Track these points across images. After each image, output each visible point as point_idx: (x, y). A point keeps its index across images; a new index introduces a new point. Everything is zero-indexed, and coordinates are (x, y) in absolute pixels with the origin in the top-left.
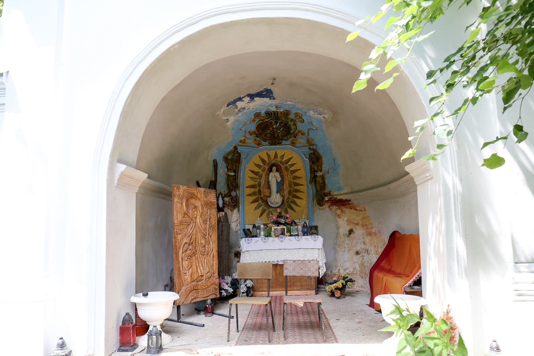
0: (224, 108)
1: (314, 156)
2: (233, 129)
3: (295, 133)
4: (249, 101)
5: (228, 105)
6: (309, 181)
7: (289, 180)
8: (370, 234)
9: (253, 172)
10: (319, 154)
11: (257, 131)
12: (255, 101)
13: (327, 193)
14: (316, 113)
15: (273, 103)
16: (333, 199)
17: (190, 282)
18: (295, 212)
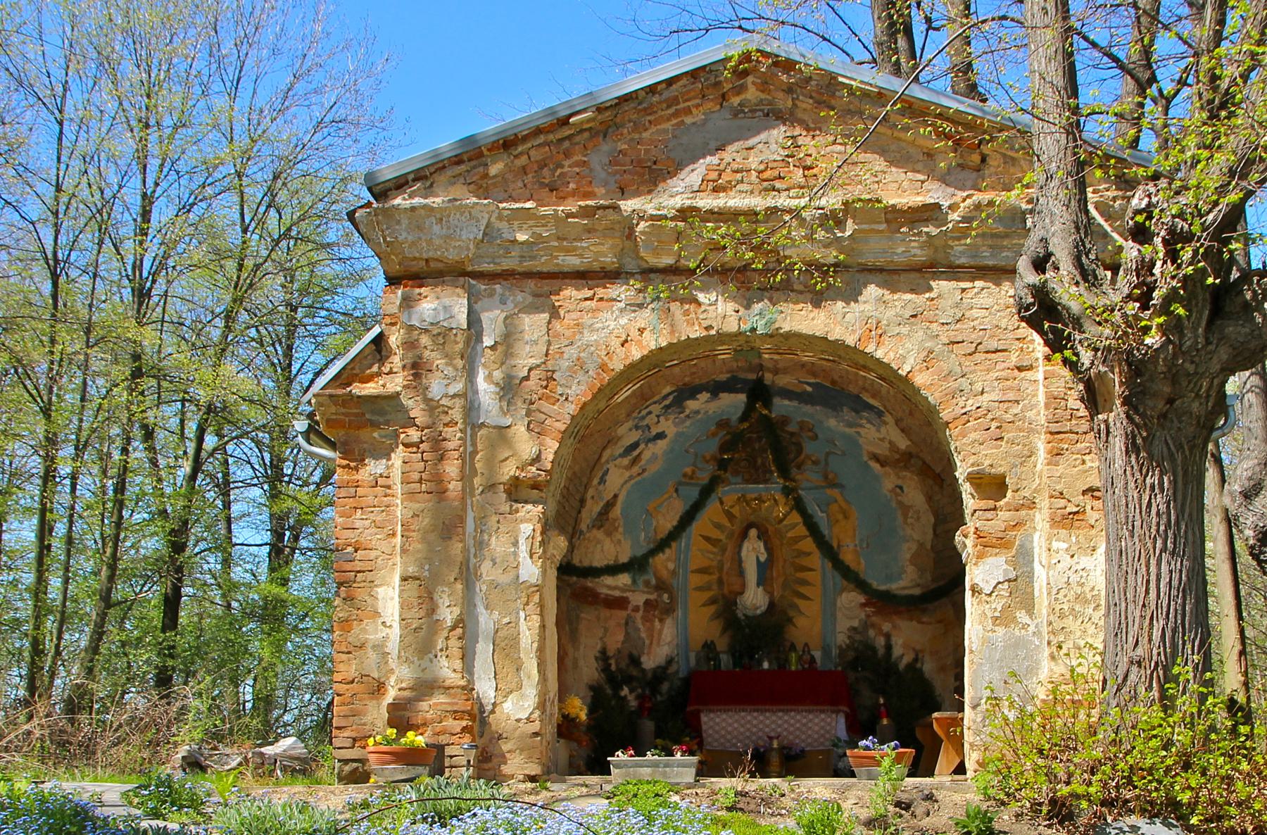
9: (707, 539)
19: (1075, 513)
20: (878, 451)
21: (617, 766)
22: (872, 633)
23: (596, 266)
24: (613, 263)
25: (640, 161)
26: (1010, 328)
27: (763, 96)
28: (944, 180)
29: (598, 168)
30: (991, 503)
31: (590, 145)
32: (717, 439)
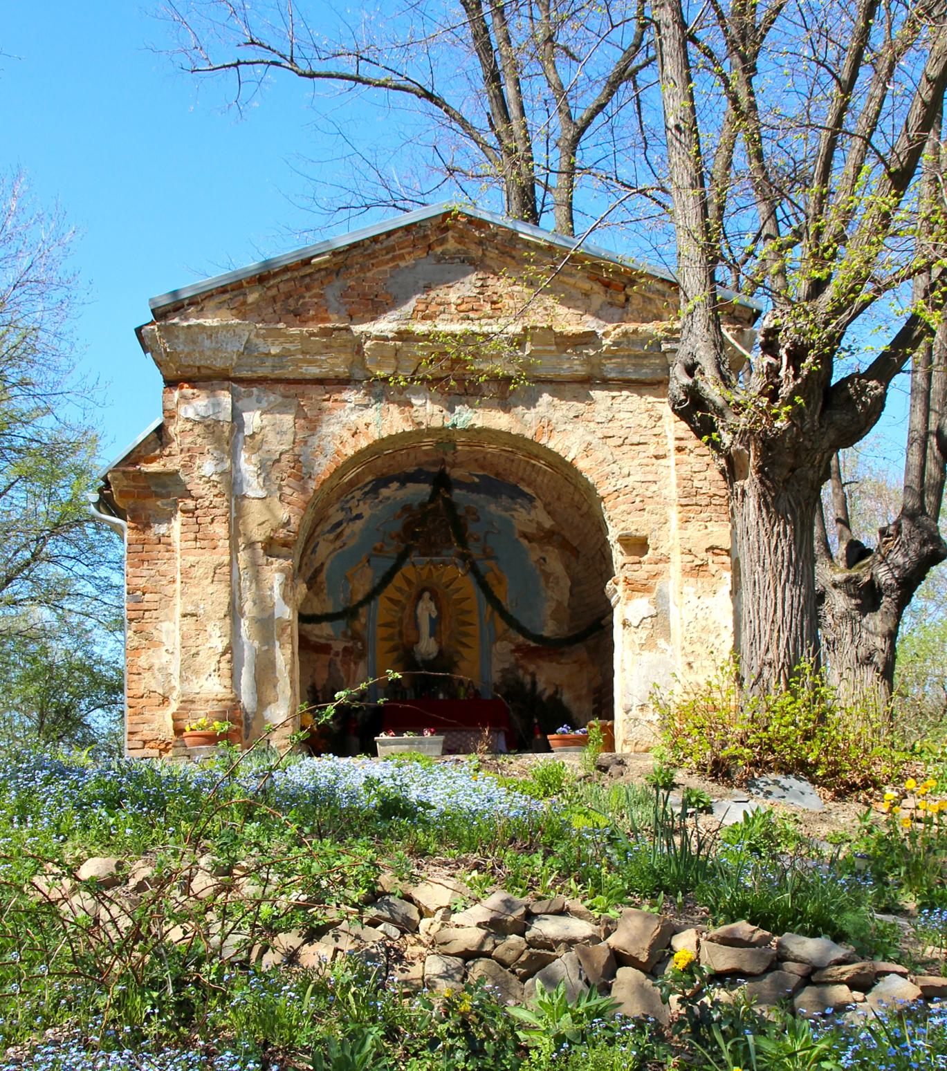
19: (700, 566)
20: (528, 530)
21: (383, 744)
22: (521, 672)
23: (331, 375)
24: (345, 372)
25: (365, 295)
26: (649, 426)
27: (460, 247)
28: (597, 315)
29: (332, 299)
30: (636, 559)
31: (326, 281)
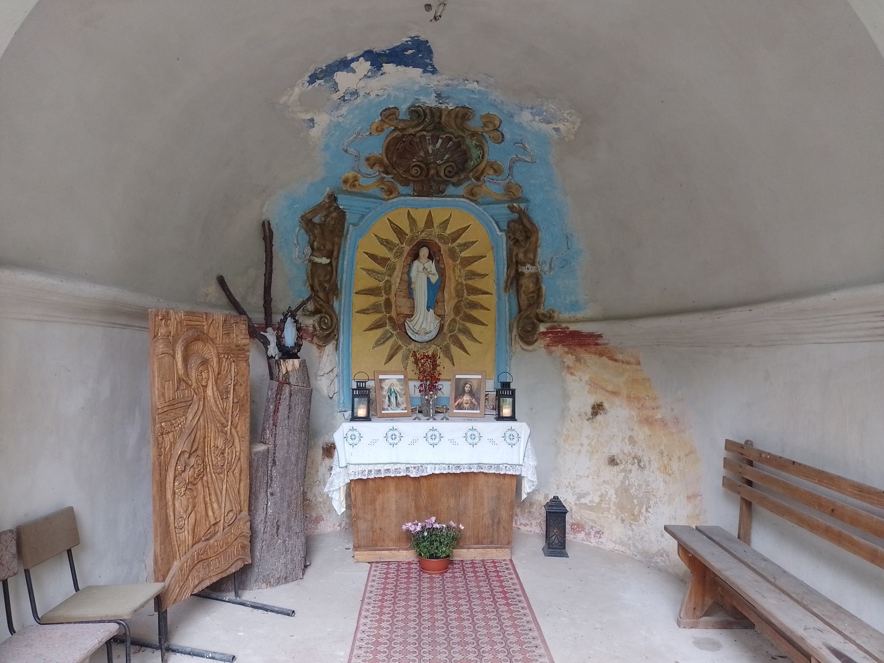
0: (301, 87)
1: (521, 227)
2: (327, 147)
3: (479, 167)
4: (370, 73)
5: (313, 79)
6: (502, 285)
7: (457, 281)
8: (648, 421)
9: (373, 257)
10: (532, 223)
11: (388, 159)
12: (384, 73)
13: (543, 315)
14: (537, 118)
15: (432, 85)
16: (559, 330)
17: (190, 546)
18: (468, 354)
32: (383, 135)
